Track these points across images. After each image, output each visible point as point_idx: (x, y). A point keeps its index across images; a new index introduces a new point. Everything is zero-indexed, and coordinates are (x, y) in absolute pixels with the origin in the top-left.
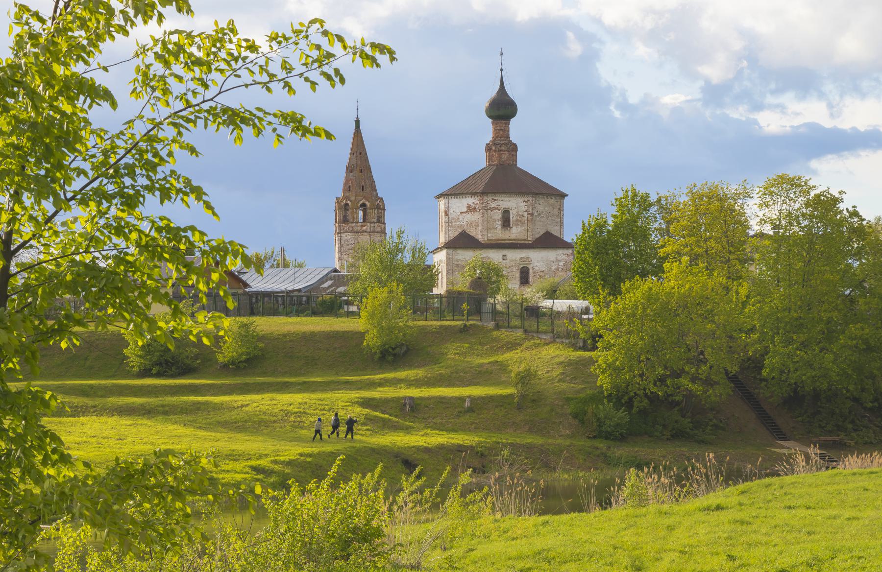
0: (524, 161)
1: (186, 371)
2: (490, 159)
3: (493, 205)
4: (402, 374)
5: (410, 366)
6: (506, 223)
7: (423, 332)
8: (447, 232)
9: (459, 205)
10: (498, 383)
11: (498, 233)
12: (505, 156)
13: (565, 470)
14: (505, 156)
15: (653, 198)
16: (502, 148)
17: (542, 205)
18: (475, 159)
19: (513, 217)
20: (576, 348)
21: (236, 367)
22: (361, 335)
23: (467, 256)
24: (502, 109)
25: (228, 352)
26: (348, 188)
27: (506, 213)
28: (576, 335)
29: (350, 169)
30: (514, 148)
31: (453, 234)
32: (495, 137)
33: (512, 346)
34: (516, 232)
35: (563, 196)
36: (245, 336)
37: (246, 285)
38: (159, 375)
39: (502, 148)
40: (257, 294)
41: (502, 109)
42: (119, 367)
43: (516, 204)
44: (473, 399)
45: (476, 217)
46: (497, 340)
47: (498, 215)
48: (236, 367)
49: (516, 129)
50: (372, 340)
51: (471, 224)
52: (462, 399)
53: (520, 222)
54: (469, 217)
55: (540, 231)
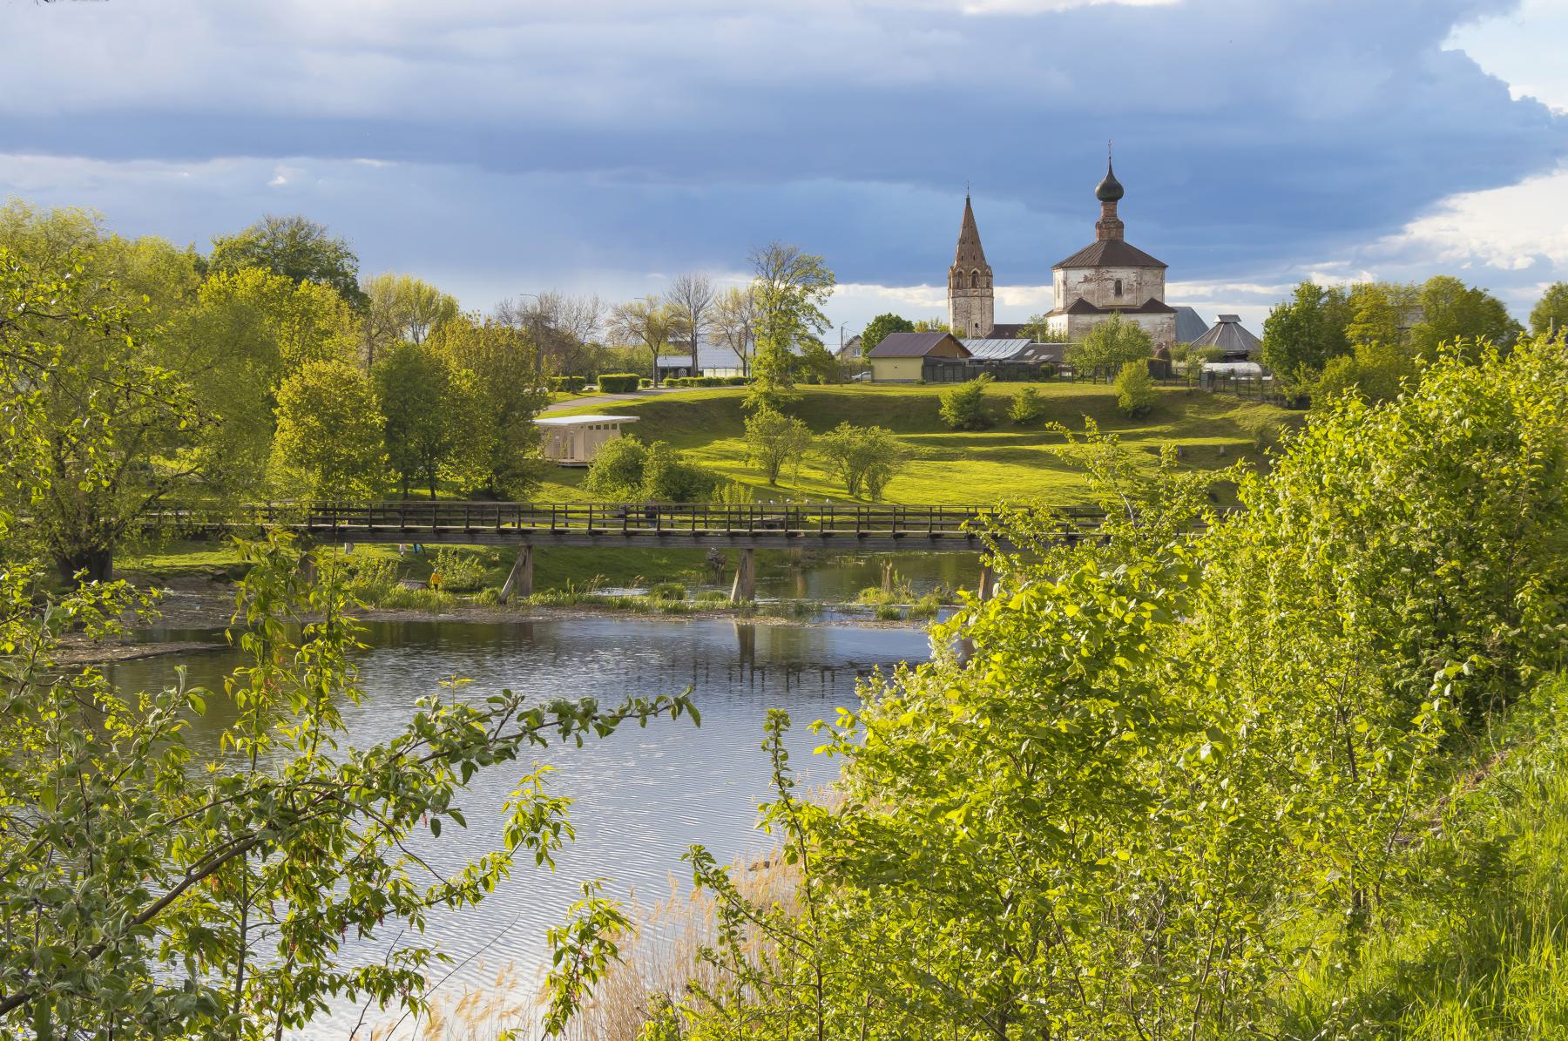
0: (1128, 239)
1: (987, 425)
2: (1101, 235)
3: (1107, 276)
4: (1157, 429)
5: (1163, 423)
6: (1118, 291)
7: (1163, 395)
8: (1066, 299)
9: (1077, 276)
10: (1229, 435)
11: (1112, 300)
12: (1113, 233)
13: (762, 596)
14: (1113, 233)
15: (1325, 289)
16: (1111, 227)
17: (1148, 276)
18: (1087, 235)
19: (1124, 286)
20: (1290, 407)
21: (1022, 424)
22: (1114, 400)
23: (1083, 319)
24: (1111, 192)
25: (1019, 411)
26: (961, 259)
27: (1118, 283)
28: (1283, 398)
29: (962, 241)
30: (1121, 226)
31: (1072, 300)
32: (1106, 216)
33: (1232, 406)
34: (1127, 299)
35: (1165, 267)
36: (1033, 400)
37: (968, 354)
38: (969, 430)
39: (1111, 227)
40: (980, 362)
41: (1111, 192)
42: (938, 424)
43: (1127, 275)
44: (1226, 447)
45: (1092, 286)
46: (1217, 402)
47: (1111, 285)
48: (1022, 424)
49: (1122, 209)
50: (1126, 401)
51: (1088, 292)
52: (1217, 447)
53: (1130, 290)
54: (1085, 286)
55: (1146, 298)
